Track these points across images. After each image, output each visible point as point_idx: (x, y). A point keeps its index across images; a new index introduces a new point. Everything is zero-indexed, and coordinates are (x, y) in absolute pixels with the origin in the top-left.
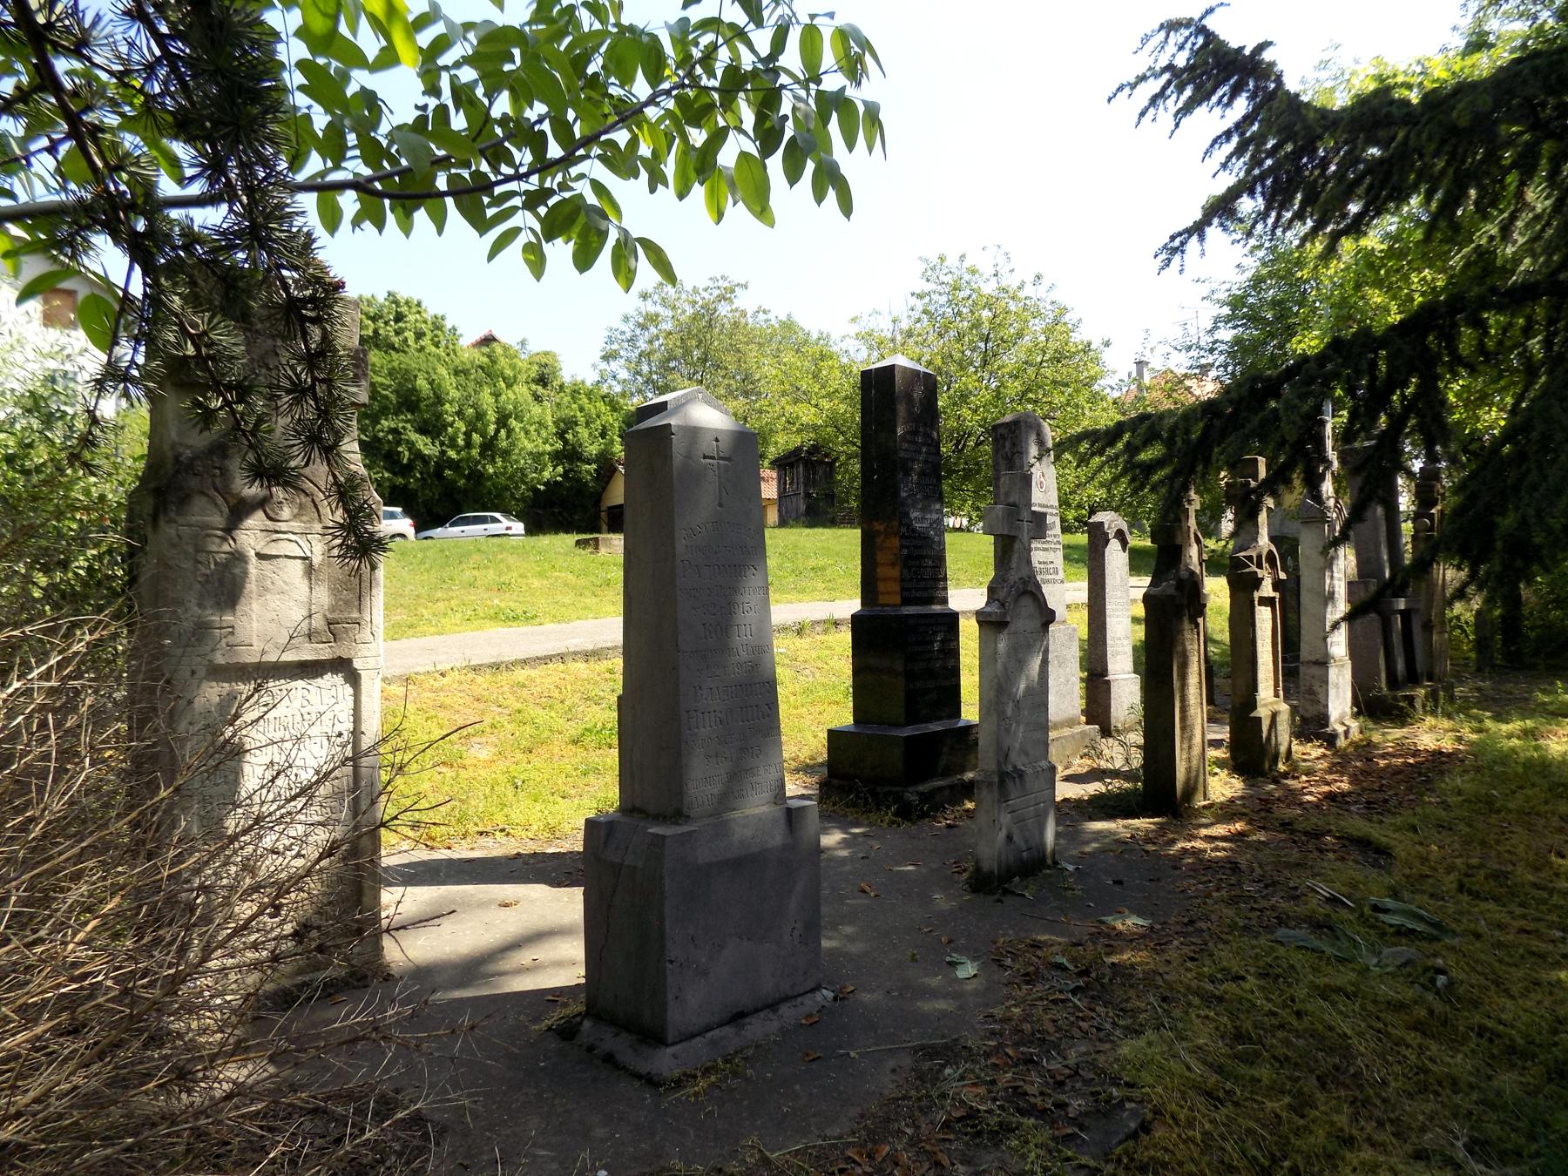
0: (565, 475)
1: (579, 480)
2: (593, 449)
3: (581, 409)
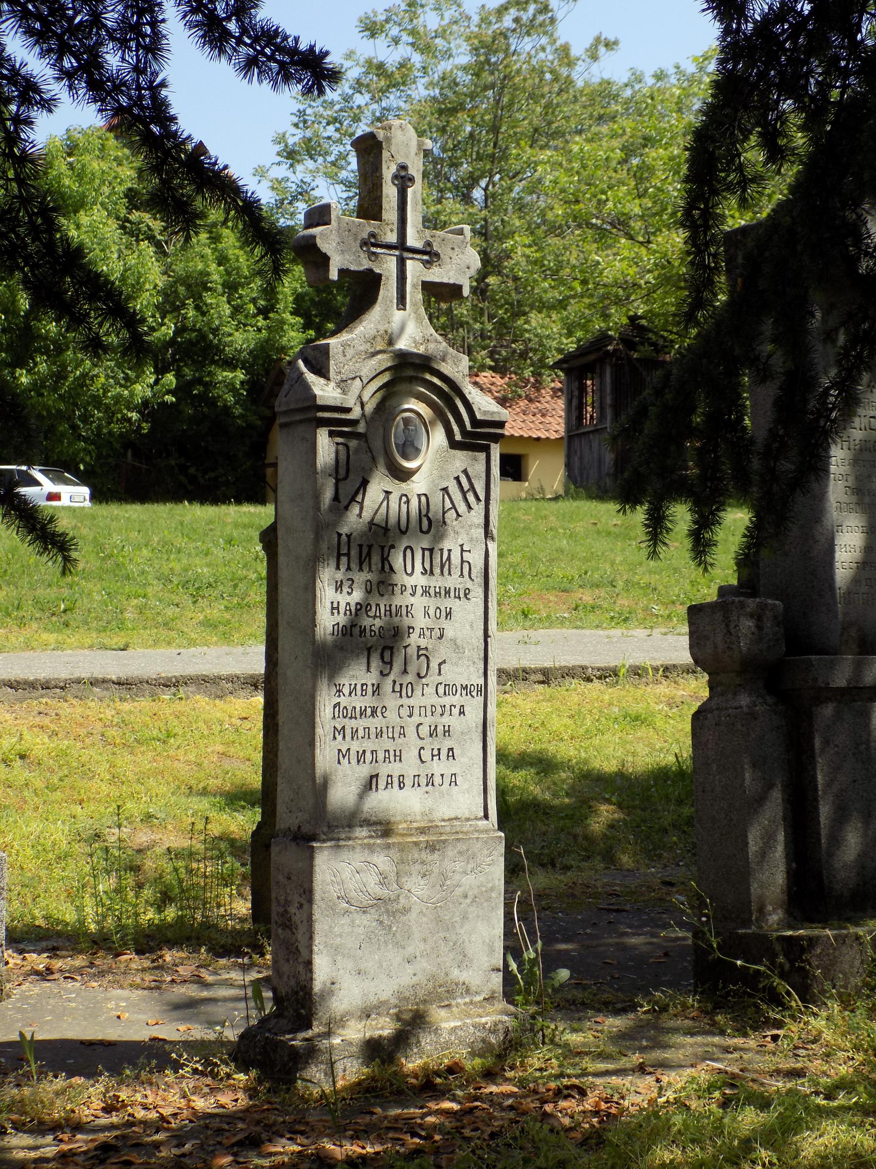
0: (181, 391)
1: (212, 402)
2: (241, 339)
3: (222, 260)
